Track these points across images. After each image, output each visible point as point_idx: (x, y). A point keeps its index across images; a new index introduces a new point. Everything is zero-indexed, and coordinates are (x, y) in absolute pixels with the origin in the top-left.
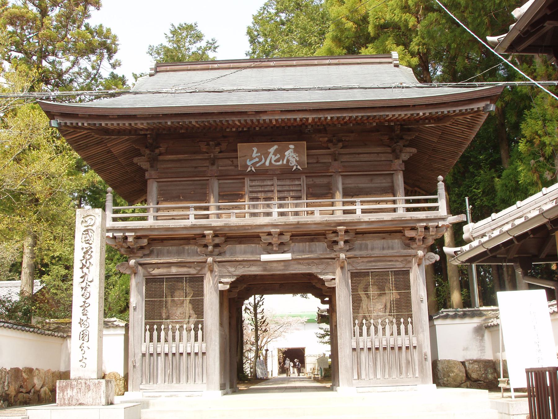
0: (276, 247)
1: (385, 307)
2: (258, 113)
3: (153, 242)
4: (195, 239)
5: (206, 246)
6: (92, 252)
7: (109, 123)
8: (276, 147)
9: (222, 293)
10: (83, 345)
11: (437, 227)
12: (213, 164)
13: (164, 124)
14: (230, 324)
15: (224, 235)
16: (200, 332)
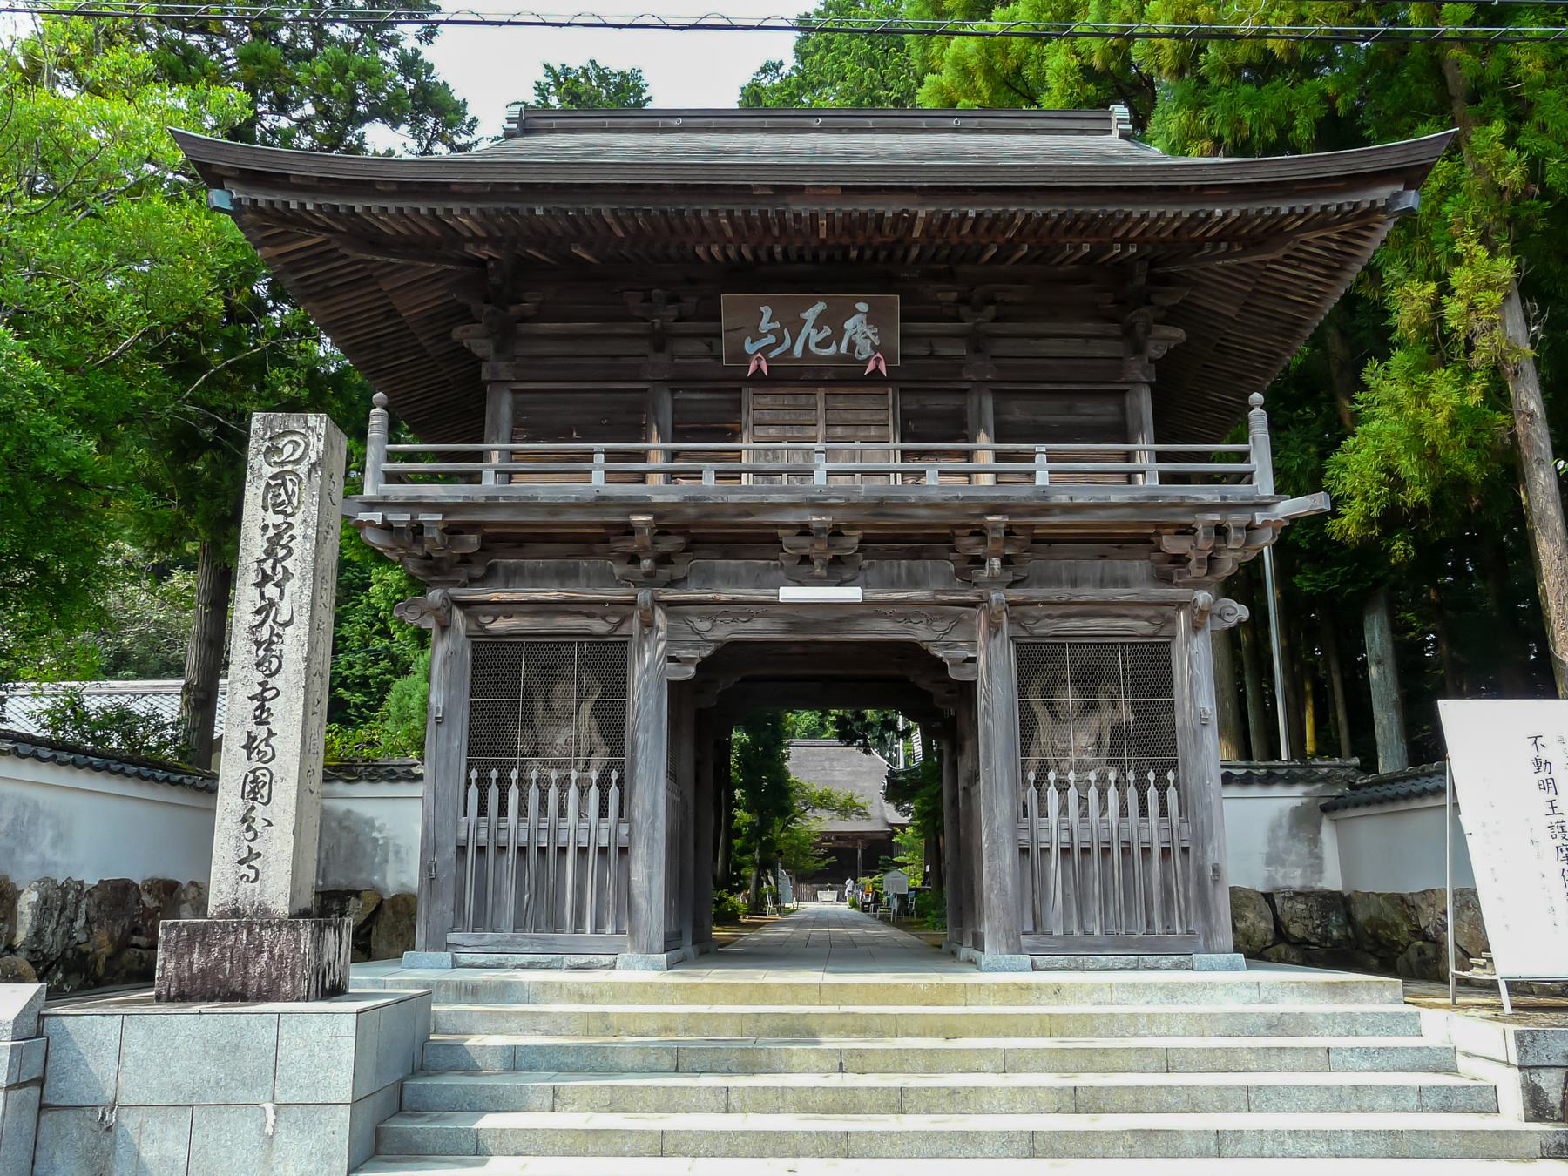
0: (822, 566)
1: (1099, 742)
2: (781, 190)
3: (498, 544)
4: (607, 541)
5: (634, 559)
6: (292, 538)
7: (375, 205)
8: (820, 307)
9: (675, 688)
10: (253, 814)
11: (1251, 527)
12: (659, 348)
13: (525, 213)
14: (697, 779)
15: (682, 529)
16: (614, 792)
